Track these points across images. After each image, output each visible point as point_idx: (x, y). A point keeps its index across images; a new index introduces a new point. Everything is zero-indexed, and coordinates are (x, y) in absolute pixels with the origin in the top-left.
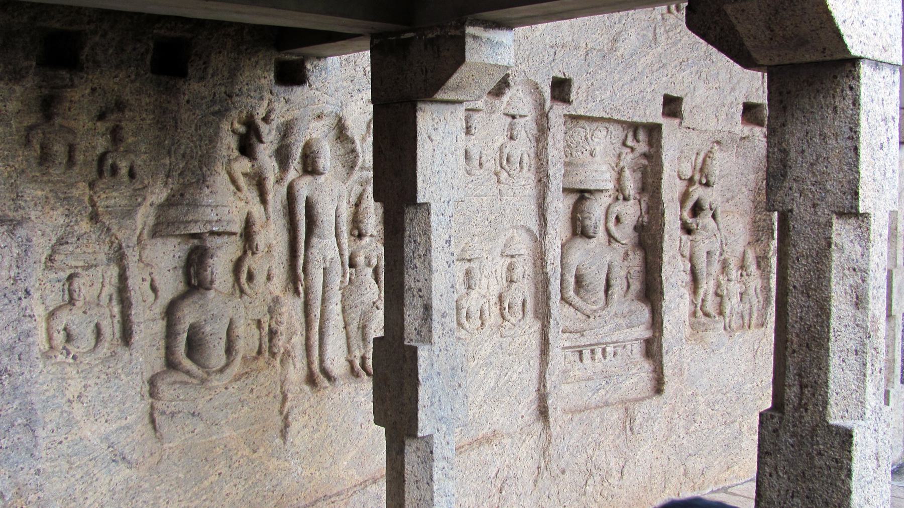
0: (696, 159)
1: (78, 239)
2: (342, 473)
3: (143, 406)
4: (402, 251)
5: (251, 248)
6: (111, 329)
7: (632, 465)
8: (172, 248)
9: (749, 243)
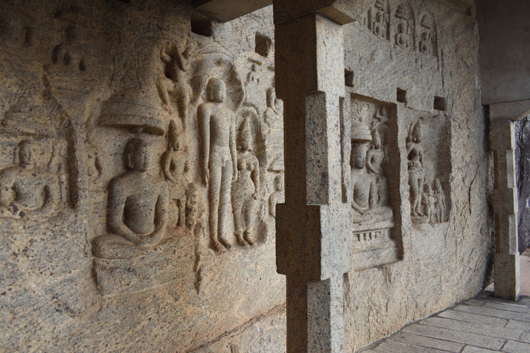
0: (410, 128)
1: (31, 110)
2: (236, 314)
3: (86, 262)
4: (304, 131)
5: (173, 146)
6: (58, 193)
7: (392, 302)
8: (114, 137)
9: (436, 176)
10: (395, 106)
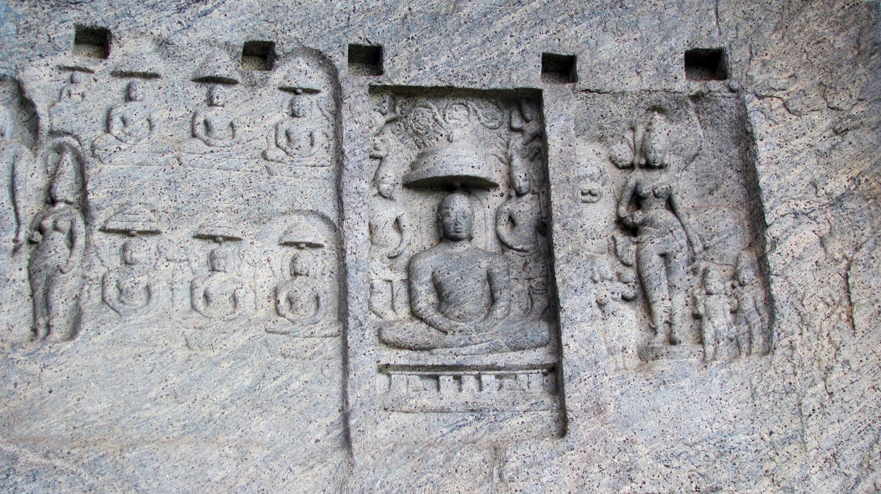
9: (750, 245)
10: (539, 92)
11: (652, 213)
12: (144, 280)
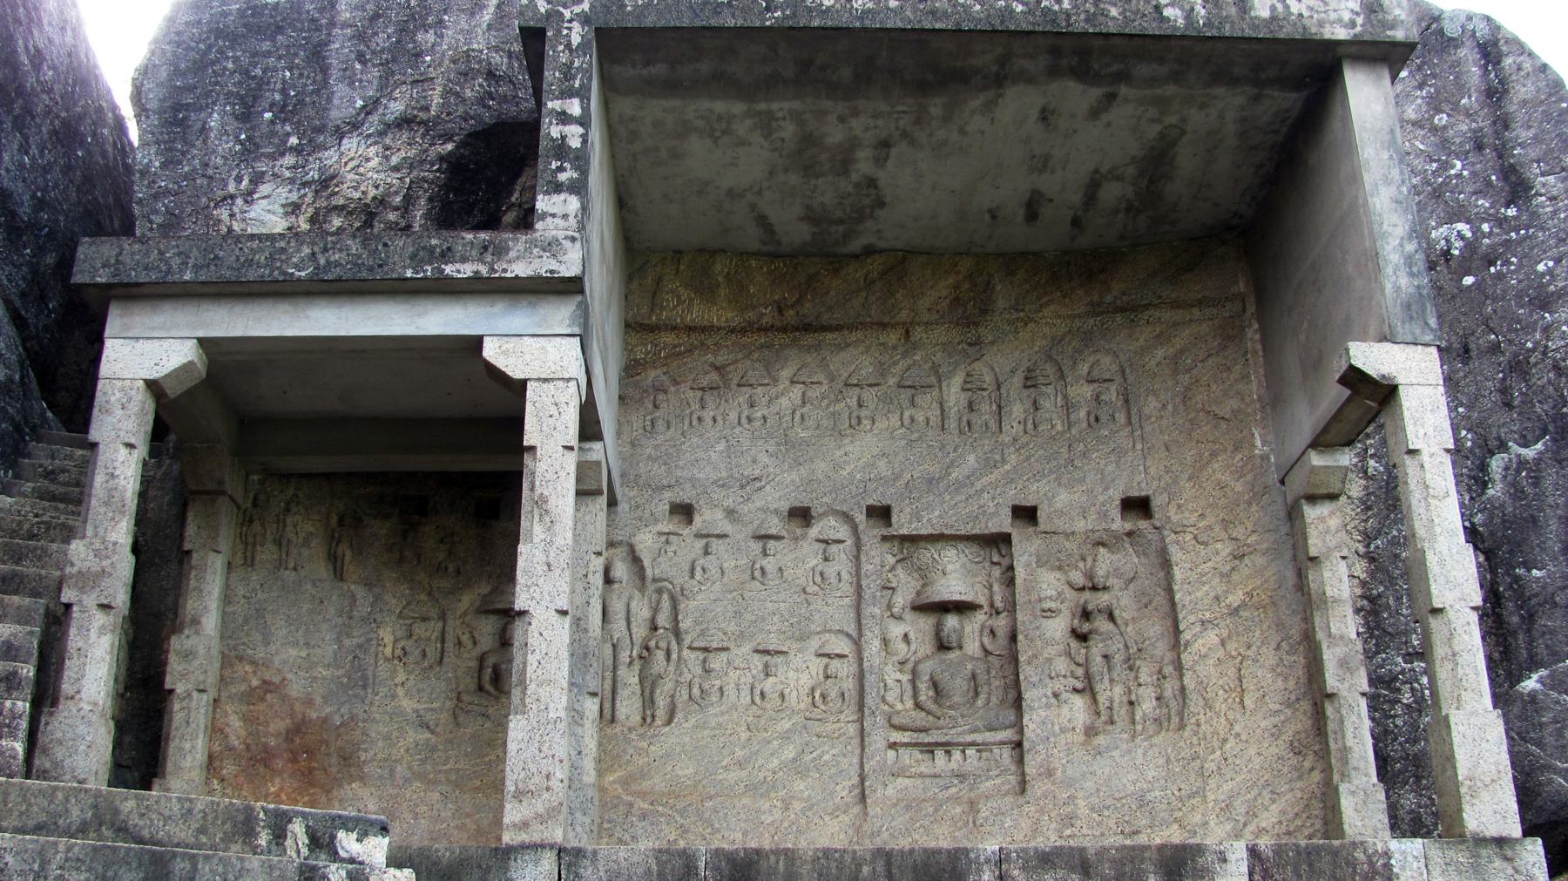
6: (432, 653)
11: (1097, 624)
12: (718, 683)
